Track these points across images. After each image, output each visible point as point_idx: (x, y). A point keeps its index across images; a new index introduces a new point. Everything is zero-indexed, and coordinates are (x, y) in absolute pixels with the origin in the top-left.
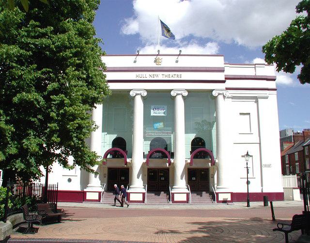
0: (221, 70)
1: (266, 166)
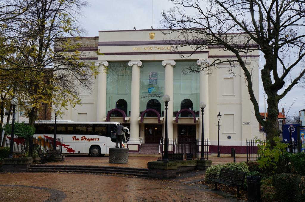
1: (245, 123)
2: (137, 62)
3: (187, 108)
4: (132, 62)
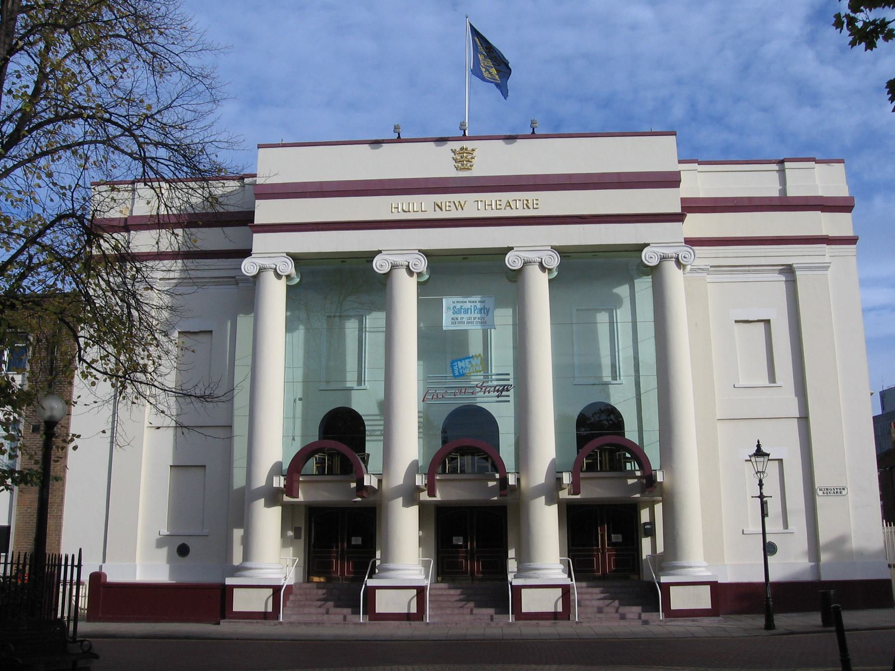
0: (671, 181)
1: (827, 491)
2: (275, 261)
3: (598, 434)
4: (518, 253)
